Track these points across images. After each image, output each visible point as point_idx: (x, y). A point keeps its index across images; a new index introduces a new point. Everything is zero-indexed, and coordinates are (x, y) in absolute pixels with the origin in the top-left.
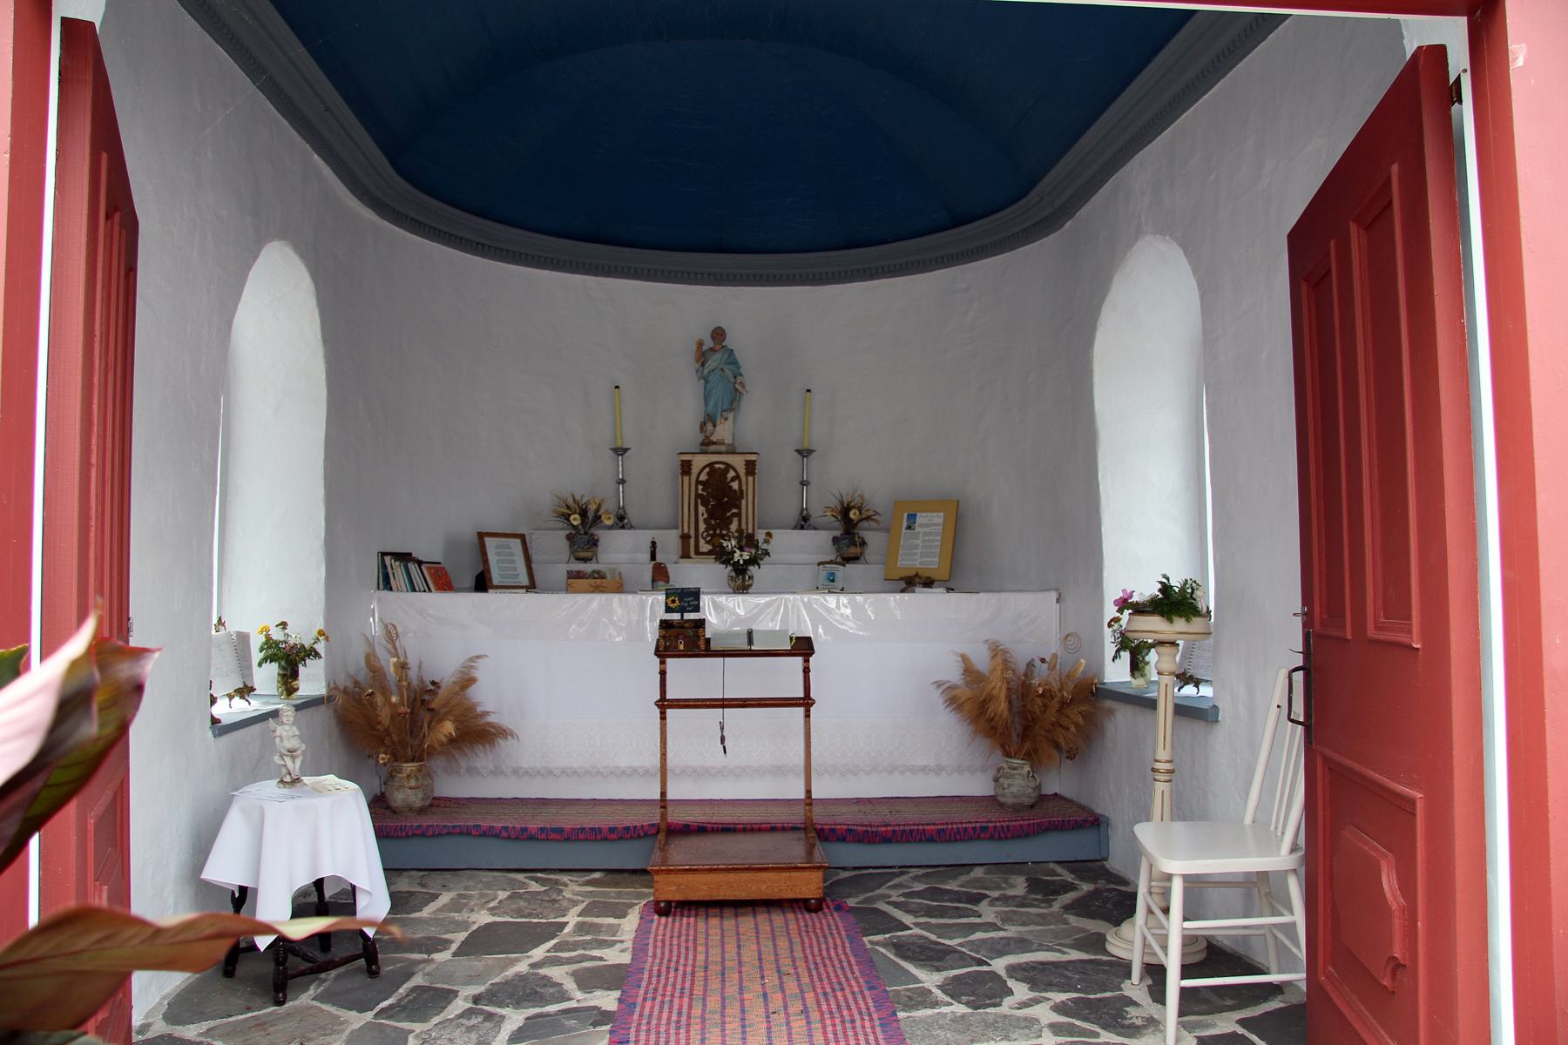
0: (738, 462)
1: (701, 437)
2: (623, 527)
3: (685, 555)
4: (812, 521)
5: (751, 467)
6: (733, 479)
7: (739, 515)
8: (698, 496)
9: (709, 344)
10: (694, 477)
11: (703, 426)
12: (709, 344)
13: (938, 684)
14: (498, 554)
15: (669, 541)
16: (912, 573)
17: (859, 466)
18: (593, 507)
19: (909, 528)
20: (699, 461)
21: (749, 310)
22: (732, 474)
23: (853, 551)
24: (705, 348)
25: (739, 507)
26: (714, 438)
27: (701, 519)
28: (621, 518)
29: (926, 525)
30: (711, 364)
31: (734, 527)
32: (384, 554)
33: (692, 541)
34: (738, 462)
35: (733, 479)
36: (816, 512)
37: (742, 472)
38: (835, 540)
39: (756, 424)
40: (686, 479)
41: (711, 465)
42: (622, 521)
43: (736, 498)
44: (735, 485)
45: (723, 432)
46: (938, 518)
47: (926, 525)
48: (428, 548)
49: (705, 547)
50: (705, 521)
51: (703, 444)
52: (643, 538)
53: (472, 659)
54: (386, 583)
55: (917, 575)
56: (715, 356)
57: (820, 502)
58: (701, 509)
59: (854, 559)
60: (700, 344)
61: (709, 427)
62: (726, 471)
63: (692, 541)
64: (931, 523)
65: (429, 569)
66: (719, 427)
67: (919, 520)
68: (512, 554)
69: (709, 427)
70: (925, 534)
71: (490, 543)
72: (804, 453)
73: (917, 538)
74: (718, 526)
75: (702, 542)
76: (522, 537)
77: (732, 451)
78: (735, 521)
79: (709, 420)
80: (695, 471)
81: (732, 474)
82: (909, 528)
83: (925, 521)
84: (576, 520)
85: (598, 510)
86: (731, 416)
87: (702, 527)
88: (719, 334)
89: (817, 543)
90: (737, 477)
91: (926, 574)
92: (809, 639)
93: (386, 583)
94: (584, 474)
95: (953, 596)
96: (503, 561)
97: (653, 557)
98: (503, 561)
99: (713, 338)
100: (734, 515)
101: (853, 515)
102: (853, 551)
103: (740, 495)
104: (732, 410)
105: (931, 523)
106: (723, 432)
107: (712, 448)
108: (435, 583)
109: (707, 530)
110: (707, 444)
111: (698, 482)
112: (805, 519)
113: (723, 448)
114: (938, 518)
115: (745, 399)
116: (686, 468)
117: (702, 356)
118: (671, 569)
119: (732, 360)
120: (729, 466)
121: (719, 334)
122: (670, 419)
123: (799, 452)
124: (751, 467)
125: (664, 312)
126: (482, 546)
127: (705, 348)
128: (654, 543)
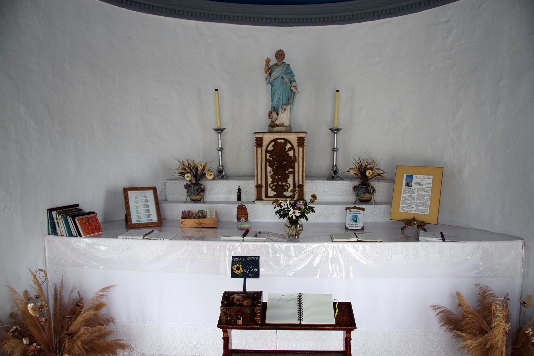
0: (293, 138)
1: (269, 122)
2: (223, 178)
3: (259, 198)
4: (340, 174)
5: (301, 142)
6: (290, 150)
7: (293, 173)
8: (267, 160)
9: (273, 61)
10: (264, 148)
11: (270, 114)
12: (273, 61)
13: (435, 307)
14: (137, 202)
15: (249, 188)
16: (410, 217)
17: (371, 138)
18: (200, 168)
19: (407, 185)
20: (268, 138)
21: (298, 40)
22: (289, 146)
23: (367, 196)
24: (271, 64)
25: (293, 168)
26: (277, 122)
27: (269, 175)
28: (221, 172)
29: (419, 184)
30: (275, 74)
31: (290, 180)
32: (50, 210)
33: (263, 189)
34: (293, 138)
35: (290, 150)
36: (342, 168)
37: (295, 144)
38: (355, 188)
39: (305, 114)
40: (259, 149)
41: (275, 140)
42: (221, 174)
43: (292, 162)
44: (291, 153)
45: (283, 118)
46: (429, 179)
47: (419, 184)
48: (92, 200)
49: (271, 193)
50: (272, 177)
51: (270, 126)
52: (232, 185)
53: (108, 288)
54: (53, 230)
55: (414, 219)
56: (279, 72)
57: (346, 163)
58: (269, 169)
59: (367, 201)
60: (268, 61)
61: (274, 115)
62: (285, 144)
63: (263, 189)
64: (423, 182)
65: (81, 221)
66: (281, 115)
67: (414, 180)
68: (147, 201)
69: (274, 115)
70: (419, 190)
71: (131, 194)
72: (335, 131)
73: (413, 192)
74: (280, 179)
75: (270, 190)
76: (154, 189)
77: (290, 132)
78: (291, 177)
79: (275, 110)
80: (265, 144)
81: (289, 146)
82: (407, 185)
83: (419, 181)
84: (188, 177)
85: (203, 169)
86: (288, 107)
87: (270, 180)
88: (280, 55)
89: (341, 190)
90: (292, 148)
91: (420, 219)
92: (280, 50)
93: (53, 230)
94: (194, 144)
95: (447, 245)
96: (140, 207)
97: (239, 199)
98: (140, 207)
99: (276, 57)
100: (290, 173)
101: (368, 173)
102: (367, 196)
103: (294, 159)
104: (288, 104)
105: (423, 182)
106: (283, 118)
107: (276, 129)
108: (84, 231)
109: (273, 182)
110: (273, 126)
111: (267, 151)
112: (335, 172)
113: (283, 129)
114: (429, 179)
115: (297, 97)
116: (259, 142)
117: (269, 70)
118: (249, 207)
119: (289, 71)
120: (287, 141)
121: (280, 55)
122: (250, 111)
123: (331, 130)
124: (301, 142)
125: (255, 41)
126: (126, 197)
127: (271, 64)
128: (239, 190)
